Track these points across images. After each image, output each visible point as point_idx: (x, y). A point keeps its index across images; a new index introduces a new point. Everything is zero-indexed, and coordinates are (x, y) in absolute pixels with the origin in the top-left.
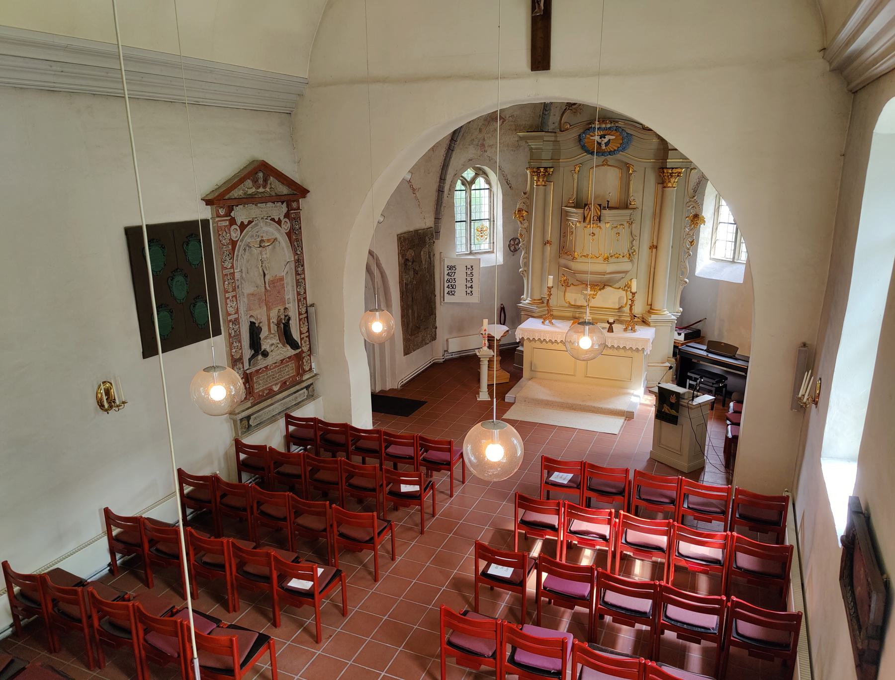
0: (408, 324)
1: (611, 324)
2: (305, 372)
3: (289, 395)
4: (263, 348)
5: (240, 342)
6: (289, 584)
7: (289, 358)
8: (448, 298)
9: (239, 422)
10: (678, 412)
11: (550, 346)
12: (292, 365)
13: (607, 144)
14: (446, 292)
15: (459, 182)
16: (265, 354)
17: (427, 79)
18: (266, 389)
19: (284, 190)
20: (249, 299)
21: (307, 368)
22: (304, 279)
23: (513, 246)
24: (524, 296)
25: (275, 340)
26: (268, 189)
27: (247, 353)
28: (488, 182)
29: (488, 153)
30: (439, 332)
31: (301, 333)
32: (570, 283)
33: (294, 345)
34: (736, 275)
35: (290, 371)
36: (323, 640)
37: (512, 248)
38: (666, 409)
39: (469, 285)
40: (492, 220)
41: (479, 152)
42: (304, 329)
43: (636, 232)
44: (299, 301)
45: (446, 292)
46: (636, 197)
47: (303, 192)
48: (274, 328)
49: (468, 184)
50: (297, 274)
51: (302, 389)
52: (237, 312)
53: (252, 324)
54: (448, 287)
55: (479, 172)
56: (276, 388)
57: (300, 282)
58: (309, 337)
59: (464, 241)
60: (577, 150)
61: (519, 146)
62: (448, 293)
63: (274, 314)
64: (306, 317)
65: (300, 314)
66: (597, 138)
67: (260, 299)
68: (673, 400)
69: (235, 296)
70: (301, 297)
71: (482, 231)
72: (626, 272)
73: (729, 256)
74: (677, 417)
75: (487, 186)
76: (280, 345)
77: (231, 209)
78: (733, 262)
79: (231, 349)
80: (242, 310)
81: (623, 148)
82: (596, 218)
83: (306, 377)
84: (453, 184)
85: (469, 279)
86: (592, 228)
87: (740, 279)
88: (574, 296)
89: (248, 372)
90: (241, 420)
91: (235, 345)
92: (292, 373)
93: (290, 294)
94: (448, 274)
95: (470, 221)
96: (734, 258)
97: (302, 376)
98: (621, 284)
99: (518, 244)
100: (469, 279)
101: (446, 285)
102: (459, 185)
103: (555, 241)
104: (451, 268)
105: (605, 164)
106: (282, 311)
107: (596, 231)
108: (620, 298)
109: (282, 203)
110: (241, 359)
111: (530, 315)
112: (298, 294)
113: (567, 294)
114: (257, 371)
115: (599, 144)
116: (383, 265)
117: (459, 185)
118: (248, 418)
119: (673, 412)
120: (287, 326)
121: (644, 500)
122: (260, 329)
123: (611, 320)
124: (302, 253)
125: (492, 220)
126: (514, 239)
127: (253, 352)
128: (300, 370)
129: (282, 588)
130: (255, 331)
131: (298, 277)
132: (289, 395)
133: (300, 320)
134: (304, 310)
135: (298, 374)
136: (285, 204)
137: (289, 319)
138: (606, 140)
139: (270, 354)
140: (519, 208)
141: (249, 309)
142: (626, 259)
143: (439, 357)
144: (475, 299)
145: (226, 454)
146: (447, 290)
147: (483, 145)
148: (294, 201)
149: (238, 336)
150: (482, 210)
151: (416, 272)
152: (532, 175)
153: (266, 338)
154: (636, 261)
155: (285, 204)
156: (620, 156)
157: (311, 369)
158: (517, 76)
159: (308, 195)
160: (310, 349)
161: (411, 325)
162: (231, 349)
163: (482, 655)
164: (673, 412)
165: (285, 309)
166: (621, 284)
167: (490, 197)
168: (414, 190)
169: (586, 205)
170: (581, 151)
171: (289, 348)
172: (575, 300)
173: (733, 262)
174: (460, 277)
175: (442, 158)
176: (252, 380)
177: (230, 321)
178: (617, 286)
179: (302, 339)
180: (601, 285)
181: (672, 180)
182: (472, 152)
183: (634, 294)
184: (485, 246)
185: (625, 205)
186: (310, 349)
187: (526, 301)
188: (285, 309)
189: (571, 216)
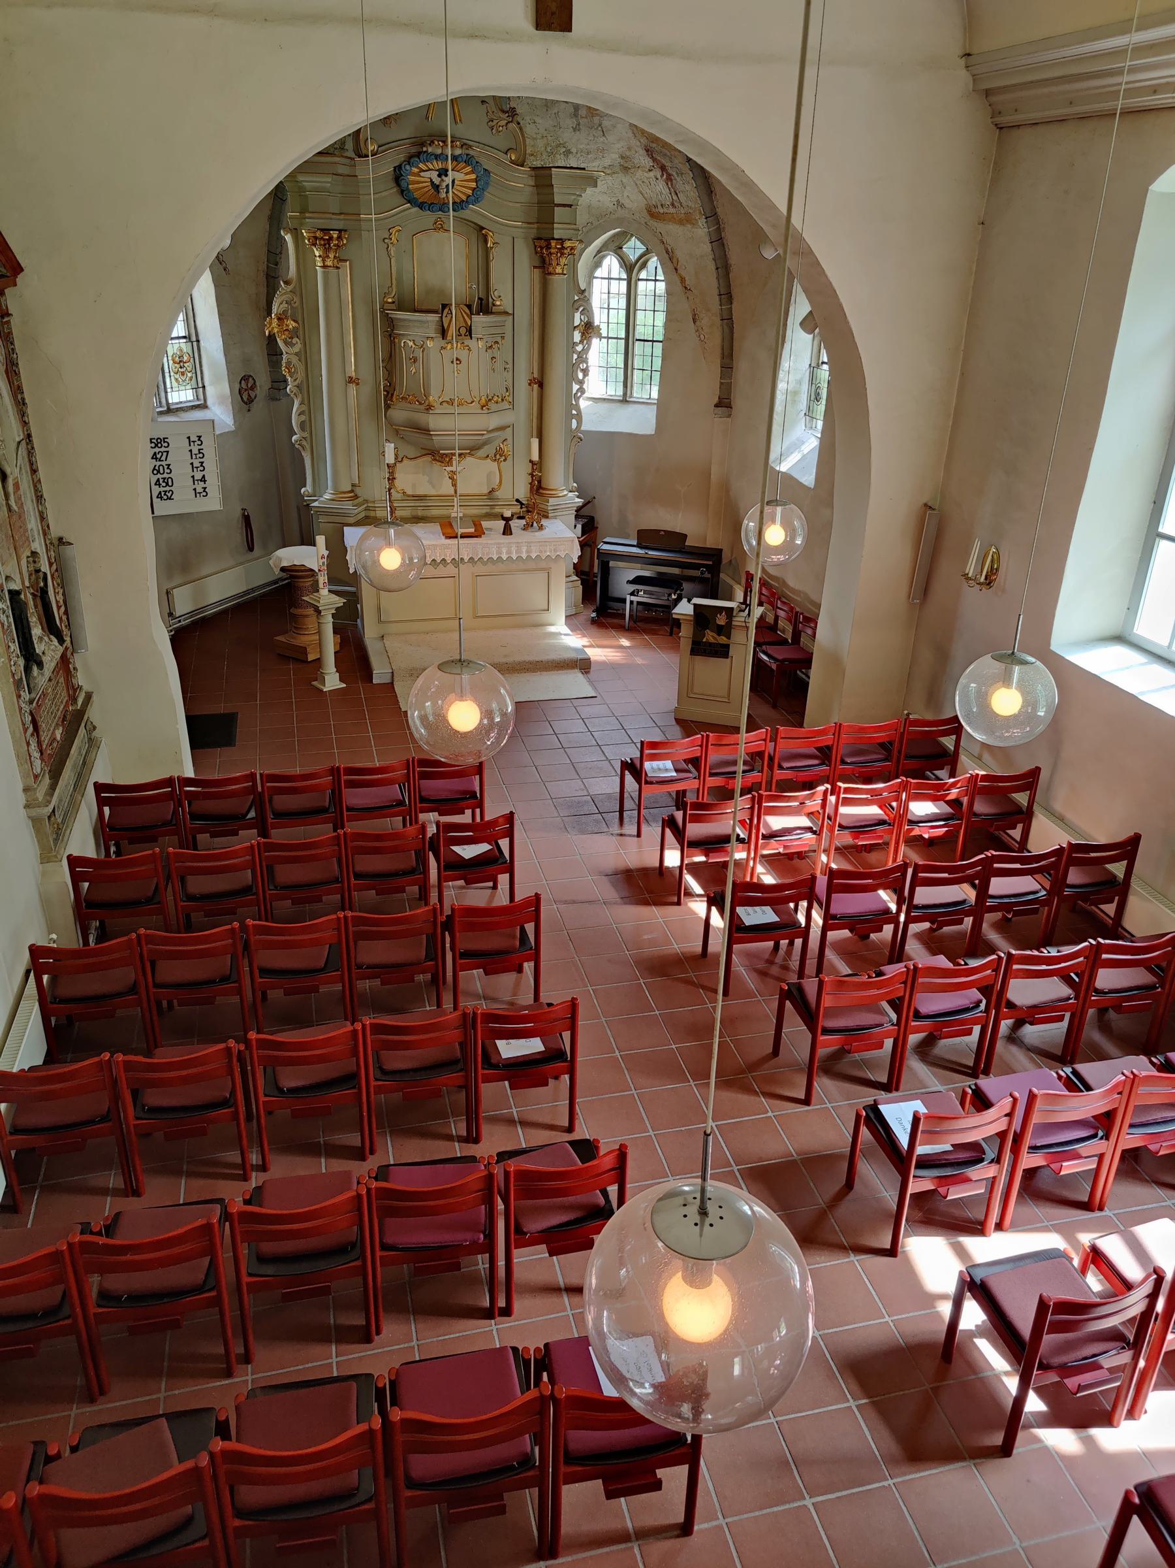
1: (507, 520)
10: (729, 638)
14: (155, 495)
23: (244, 393)
34: (640, 421)
37: (245, 397)
39: (198, 476)
45: (155, 495)
46: (502, 295)
54: (158, 483)
62: (159, 496)
64: (64, 582)
66: (434, 175)
68: (721, 620)
73: (616, 390)
74: (727, 646)
78: (625, 400)
81: (476, 196)
82: (463, 331)
85: (197, 464)
86: (455, 350)
88: (415, 479)
96: (625, 394)
98: (489, 450)
99: (252, 388)
100: (197, 464)
105: (440, 227)
107: (463, 355)
115: (436, 187)
119: (723, 640)
120: (44, 591)
121: (788, 768)
123: (508, 514)
126: (245, 378)
144: (213, 502)
145: (46, 903)
158: (508, 36)
164: (723, 640)
166: (489, 450)
169: (444, 306)
170: (399, 199)
172: (414, 486)
173: (625, 400)
181: (563, 261)
184: (180, 395)
185: (484, 307)
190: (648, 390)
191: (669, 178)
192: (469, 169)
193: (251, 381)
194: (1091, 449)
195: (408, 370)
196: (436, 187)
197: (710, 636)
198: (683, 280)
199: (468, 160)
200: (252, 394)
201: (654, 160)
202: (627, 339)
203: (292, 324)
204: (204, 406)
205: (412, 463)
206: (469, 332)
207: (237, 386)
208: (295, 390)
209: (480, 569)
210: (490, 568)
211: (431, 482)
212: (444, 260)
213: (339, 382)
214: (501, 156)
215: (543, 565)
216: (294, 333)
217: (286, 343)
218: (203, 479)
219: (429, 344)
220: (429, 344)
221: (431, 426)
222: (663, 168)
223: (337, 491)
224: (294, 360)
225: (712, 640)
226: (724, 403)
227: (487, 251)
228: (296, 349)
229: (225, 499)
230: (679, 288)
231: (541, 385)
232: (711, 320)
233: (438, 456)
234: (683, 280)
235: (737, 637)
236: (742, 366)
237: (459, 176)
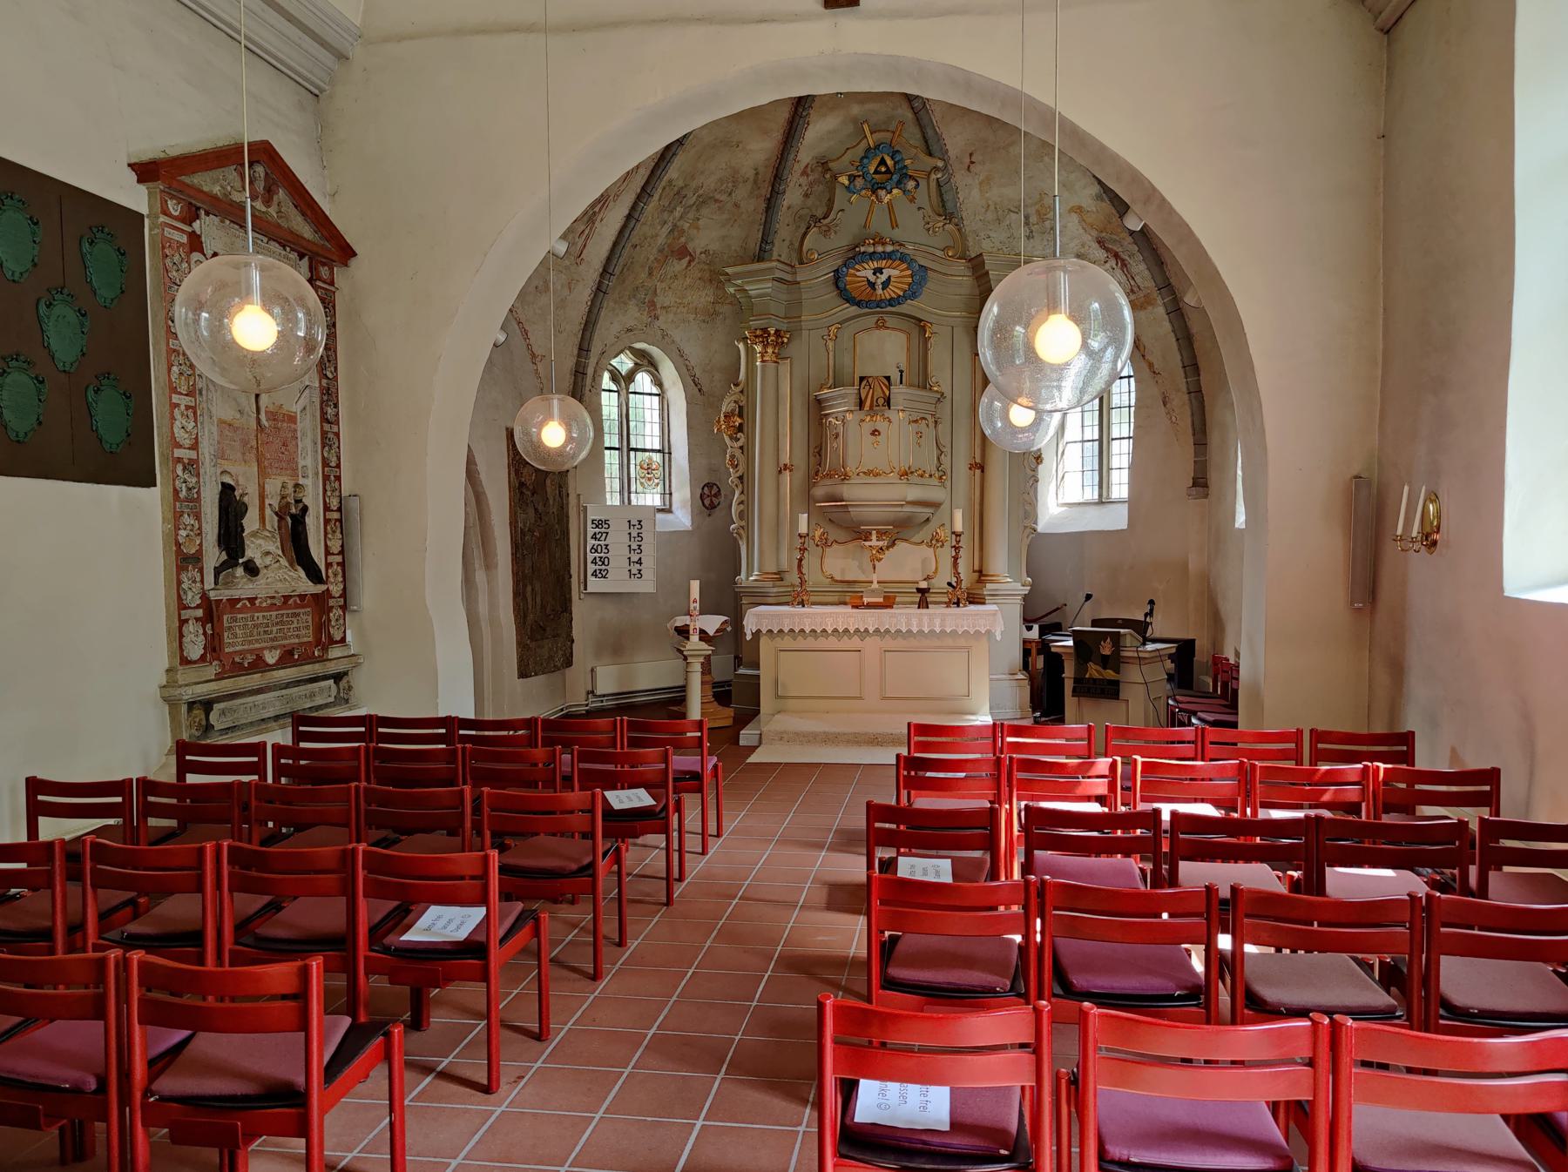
0: (525, 617)
2: (332, 642)
3: (298, 683)
4: (249, 553)
5: (198, 517)
6: (410, 936)
7: (302, 597)
8: (595, 585)
9: (184, 708)
11: (810, 643)
12: (306, 617)
13: (886, 284)
15: (606, 376)
16: (252, 570)
17: (616, 24)
18: (251, 651)
19: (307, 231)
20: (221, 433)
21: (338, 637)
22: (337, 434)
23: (709, 497)
24: (743, 575)
25: (274, 547)
26: (273, 211)
27: (213, 556)
28: (658, 382)
29: (660, 323)
30: (577, 648)
31: (328, 553)
32: (831, 539)
33: (314, 574)
35: (301, 629)
36: (504, 1087)
37: (707, 502)
38: (1094, 671)
39: (635, 558)
40: (665, 451)
41: (645, 318)
42: (335, 546)
43: (945, 441)
44: (326, 478)
45: (590, 572)
47: (346, 253)
48: (272, 520)
49: (624, 381)
50: (324, 419)
51: (325, 678)
52: (195, 446)
53: (227, 490)
55: (646, 362)
56: (271, 658)
57: (329, 440)
58: (342, 564)
59: (617, 486)
60: (831, 295)
61: (716, 313)
63: (273, 486)
64: (339, 519)
65: (327, 508)
66: (869, 274)
67: (245, 443)
68: (1106, 649)
69: (194, 409)
70: (331, 474)
71: (649, 469)
72: (936, 505)
73: (1091, 494)
74: (1116, 683)
75: (655, 390)
76: (284, 562)
77: (191, 215)
79: (177, 528)
80: (206, 449)
81: (912, 293)
82: (881, 401)
83: (335, 652)
84: (597, 378)
85: (634, 546)
87: (1122, 524)
88: (841, 563)
89: (213, 595)
90: (191, 705)
91: (187, 519)
92: (308, 636)
93: (308, 458)
94: (594, 537)
95: (627, 448)
96: (1100, 495)
97: (325, 649)
98: (925, 534)
100: (634, 546)
101: (590, 557)
102: (606, 381)
103: (801, 463)
104: (599, 524)
105: (881, 325)
106: (290, 490)
107: (881, 425)
108: (924, 561)
109: (301, 256)
110: (197, 559)
111: (760, 598)
112: (325, 463)
113: (827, 561)
114: (233, 602)
115: (872, 285)
116: (483, 477)
117: (606, 381)
118: (207, 705)
119: (1110, 674)
120: (299, 522)
122: (242, 509)
124: (336, 378)
125: (665, 451)
126: (709, 485)
127: (224, 556)
128: (324, 639)
129: (386, 949)
130: (231, 507)
131: (327, 427)
132: (298, 683)
133: (327, 522)
134: (334, 503)
135: (318, 642)
136: (306, 260)
137: (305, 509)
138: (883, 278)
139: (263, 572)
140: (721, 416)
141: (220, 455)
142: (935, 481)
143: (578, 700)
144: (647, 585)
146: (591, 568)
147: (652, 304)
148: (324, 264)
149: (194, 501)
150: (648, 435)
151: (539, 515)
152: (750, 352)
153: (254, 534)
154: (948, 484)
155: (306, 260)
156: (907, 307)
157: (343, 640)
159: (353, 262)
160: (344, 594)
161: (531, 617)
162: (177, 528)
163: (992, 990)
164: (1110, 674)
165: (297, 486)
167: (662, 410)
168: (533, 356)
171: (302, 573)
172: (843, 571)
174: (618, 541)
175: (584, 309)
176: (220, 619)
177: (179, 460)
178: (917, 539)
179: (328, 565)
180: (899, 529)
182: (633, 314)
183: (958, 535)
184: (652, 499)
186: (344, 594)
187: (748, 578)
188: (297, 486)
189: (831, 407)
190: (1120, 487)
191: (1124, 265)
192: (904, 266)
193: (715, 490)
194: (1511, 302)
195: (830, 445)
196: (872, 285)
197: (1094, 671)
198: (1151, 365)
199: (903, 258)
200: (716, 501)
201: (1107, 250)
202: (1100, 440)
203: (738, 421)
204: (669, 511)
205: (841, 547)
206: (888, 402)
207: (699, 491)
208: (737, 481)
209: (889, 643)
210: (899, 643)
211: (860, 567)
212: (886, 350)
213: (771, 470)
214: (939, 253)
215: (962, 642)
216: (740, 429)
217: (731, 438)
218: (639, 562)
219: (849, 417)
220: (849, 417)
221: (846, 496)
222: (1116, 256)
223: (762, 573)
224: (738, 453)
225: (1096, 676)
226: (1200, 482)
227: (926, 340)
228: (740, 443)
229: (659, 584)
230: (1146, 372)
231: (982, 468)
232: (1180, 400)
233: (858, 533)
234: (1151, 365)
235: (1133, 675)
236: (1214, 438)
237: (895, 273)
